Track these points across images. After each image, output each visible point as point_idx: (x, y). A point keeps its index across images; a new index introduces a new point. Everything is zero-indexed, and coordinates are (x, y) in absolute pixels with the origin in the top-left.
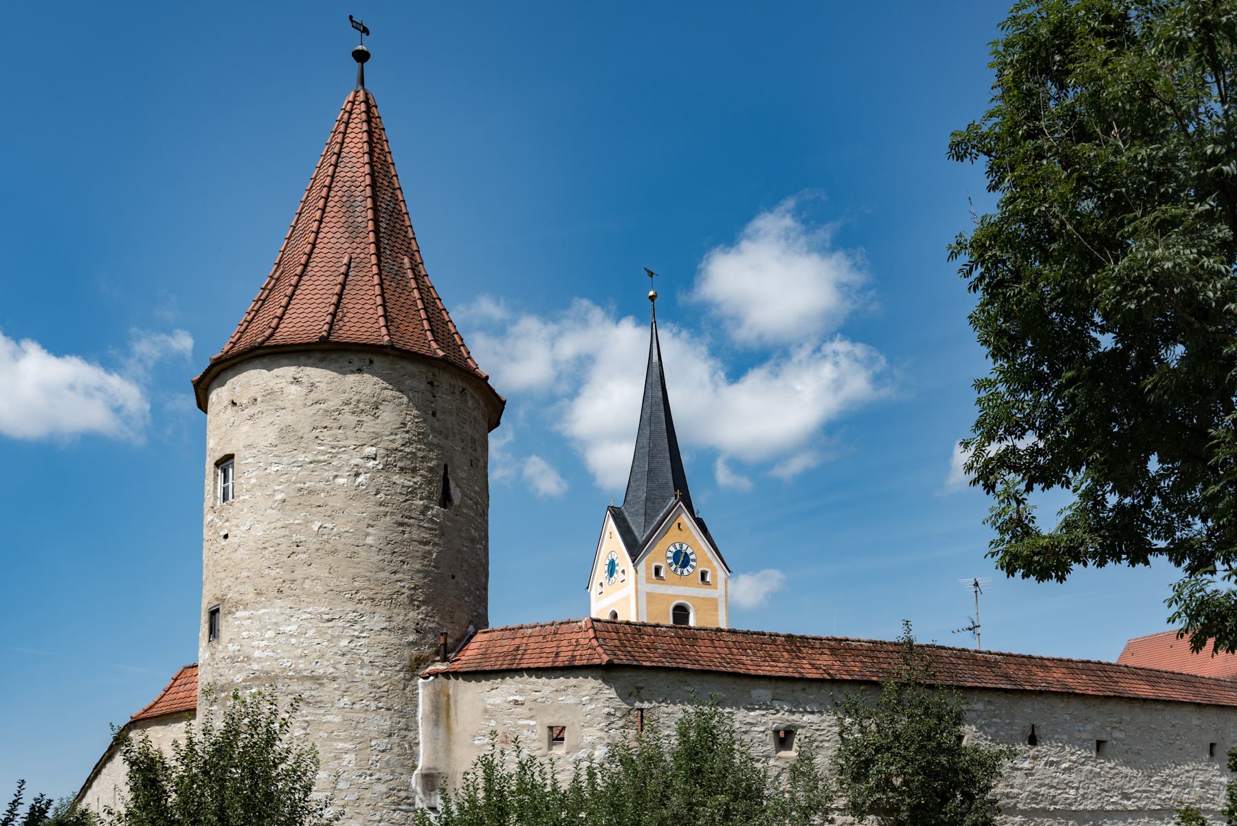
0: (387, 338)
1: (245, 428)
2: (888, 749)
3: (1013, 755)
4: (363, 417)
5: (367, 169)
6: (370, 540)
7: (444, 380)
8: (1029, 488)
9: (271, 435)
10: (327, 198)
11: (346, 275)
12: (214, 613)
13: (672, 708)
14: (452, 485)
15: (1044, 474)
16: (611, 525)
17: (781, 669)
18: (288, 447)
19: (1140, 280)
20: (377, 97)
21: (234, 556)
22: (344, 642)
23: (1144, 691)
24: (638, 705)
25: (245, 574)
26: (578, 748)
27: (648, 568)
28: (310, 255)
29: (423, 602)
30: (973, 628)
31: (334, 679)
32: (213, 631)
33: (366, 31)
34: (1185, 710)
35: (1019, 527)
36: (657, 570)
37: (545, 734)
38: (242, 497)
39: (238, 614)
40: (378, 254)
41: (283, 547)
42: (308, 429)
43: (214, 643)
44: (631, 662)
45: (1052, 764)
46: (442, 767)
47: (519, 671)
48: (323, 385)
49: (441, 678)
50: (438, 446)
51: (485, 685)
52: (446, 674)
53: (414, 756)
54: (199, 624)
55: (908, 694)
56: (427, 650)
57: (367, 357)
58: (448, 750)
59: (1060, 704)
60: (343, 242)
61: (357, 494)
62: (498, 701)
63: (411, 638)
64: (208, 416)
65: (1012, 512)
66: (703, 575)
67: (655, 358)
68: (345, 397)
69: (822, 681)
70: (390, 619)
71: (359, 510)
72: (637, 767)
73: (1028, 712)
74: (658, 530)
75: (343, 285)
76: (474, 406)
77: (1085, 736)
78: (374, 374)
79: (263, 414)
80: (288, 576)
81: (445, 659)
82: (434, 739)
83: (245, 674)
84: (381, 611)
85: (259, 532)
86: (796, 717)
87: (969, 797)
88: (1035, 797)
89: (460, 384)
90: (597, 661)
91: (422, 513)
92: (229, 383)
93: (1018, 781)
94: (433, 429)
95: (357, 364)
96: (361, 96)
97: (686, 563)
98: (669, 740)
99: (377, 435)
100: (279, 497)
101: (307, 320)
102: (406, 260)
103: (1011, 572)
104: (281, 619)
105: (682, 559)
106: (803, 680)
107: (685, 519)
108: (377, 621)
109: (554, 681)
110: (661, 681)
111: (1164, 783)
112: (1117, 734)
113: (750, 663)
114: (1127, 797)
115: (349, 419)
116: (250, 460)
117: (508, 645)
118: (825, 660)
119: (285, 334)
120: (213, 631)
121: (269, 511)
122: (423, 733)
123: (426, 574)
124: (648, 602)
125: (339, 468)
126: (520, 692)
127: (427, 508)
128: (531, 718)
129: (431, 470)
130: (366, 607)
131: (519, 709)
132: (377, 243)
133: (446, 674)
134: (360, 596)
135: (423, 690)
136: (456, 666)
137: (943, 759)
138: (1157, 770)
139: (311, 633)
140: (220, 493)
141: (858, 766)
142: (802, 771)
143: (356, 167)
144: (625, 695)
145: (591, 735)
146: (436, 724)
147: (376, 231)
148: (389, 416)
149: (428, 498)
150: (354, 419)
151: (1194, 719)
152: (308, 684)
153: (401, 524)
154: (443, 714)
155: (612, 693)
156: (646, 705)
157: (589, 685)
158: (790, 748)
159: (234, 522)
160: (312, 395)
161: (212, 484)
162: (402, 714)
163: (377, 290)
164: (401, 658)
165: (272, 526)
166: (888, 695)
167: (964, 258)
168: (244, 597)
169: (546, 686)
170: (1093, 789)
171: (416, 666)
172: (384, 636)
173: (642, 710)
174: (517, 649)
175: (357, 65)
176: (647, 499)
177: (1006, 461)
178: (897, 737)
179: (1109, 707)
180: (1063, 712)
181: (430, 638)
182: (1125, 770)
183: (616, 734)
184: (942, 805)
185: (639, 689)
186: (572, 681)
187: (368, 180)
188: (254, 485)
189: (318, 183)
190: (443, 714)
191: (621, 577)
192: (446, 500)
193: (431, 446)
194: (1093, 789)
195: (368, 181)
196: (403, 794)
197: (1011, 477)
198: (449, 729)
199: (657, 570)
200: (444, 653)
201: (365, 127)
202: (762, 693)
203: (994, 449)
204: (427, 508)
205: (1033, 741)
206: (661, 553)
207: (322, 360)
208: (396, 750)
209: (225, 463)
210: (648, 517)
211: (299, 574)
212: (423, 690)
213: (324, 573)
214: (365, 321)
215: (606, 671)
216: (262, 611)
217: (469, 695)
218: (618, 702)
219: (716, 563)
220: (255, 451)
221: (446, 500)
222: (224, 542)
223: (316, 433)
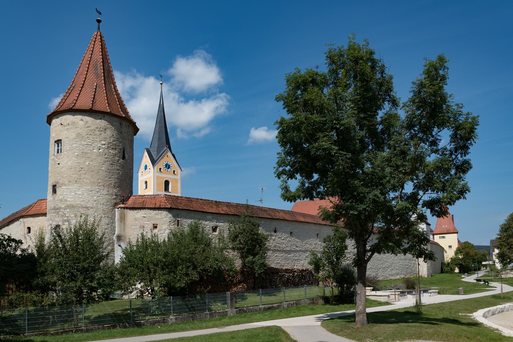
0: (109, 110)
1: (65, 132)
2: (242, 233)
3: (272, 235)
4: (102, 132)
5: (101, 57)
6: (103, 168)
7: (124, 123)
8: (288, 179)
9: (74, 135)
10: (89, 64)
11: (96, 89)
12: (54, 186)
13: (186, 220)
14: (126, 153)
15: (291, 176)
16: (146, 154)
17: (214, 211)
18: (79, 139)
19: (320, 149)
20: (104, 35)
21: (61, 170)
22: (95, 198)
23: (302, 219)
24: (178, 219)
25: (65, 175)
26: (161, 230)
27: (157, 168)
28: (84, 81)
29: (117, 187)
30: (261, 201)
31: (92, 208)
32: (54, 191)
33: (100, 13)
34: (312, 225)
35: (286, 189)
36: (160, 169)
37: (152, 227)
38: (64, 152)
39: (63, 187)
40: (105, 83)
41: (77, 169)
42: (85, 135)
43: (55, 195)
44: (177, 207)
45: (279, 238)
46: (122, 234)
47: (145, 208)
48: (90, 122)
49: (123, 209)
50: (122, 142)
51: (135, 211)
52: (124, 208)
53: (114, 231)
54: (47, 190)
55: (247, 219)
56: (118, 201)
57: (103, 115)
58: (124, 229)
59: (282, 222)
60: (95, 80)
61: (100, 155)
62: (139, 216)
63: (114, 197)
64: (51, 126)
65: (284, 185)
66: (174, 172)
67: (162, 103)
68: (96, 126)
69: (225, 214)
70: (108, 191)
71: (101, 159)
72: (176, 237)
73: (275, 224)
74: (161, 156)
75: (95, 92)
76: (131, 130)
77: (288, 231)
78: (105, 120)
79: (70, 129)
80: (79, 177)
81: (123, 204)
82: (120, 226)
84: (106, 189)
85: (70, 163)
86: (218, 224)
87: (260, 246)
88: (275, 246)
89: (128, 124)
90: (167, 207)
91: (118, 161)
92: (60, 118)
93: (271, 242)
94: (121, 137)
95: (100, 117)
96: (99, 34)
97: (169, 168)
98: (186, 229)
99: (106, 138)
100: (76, 154)
101: (85, 102)
102: (112, 86)
103: (285, 200)
104: (76, 190)
105: (168, 166)
106: (220, 214)
107: (169, 154)
108: (105, 192)
109: (155, 212)
110: (184, 213)
111: (306, 244)
112: (295, 231)
113: (207, 209)
114: (297, 247)
115: (97, 133)
117: (141, 200)
118: (225, 208)
119: (78, 106)
120: (54, 191)
122: (117, 224)
123: (118, 179)
124: (378, 290)
125: (94, 147)
126: (145, 214)
127: (119, 160)
129: (120, 149)
130: (102, 188)
131: (145, 219)
132: (104, 80)
133: (124, 208)
134: (100, 184)
135: (117, 212)
136: (127, 206)
137: (256, 237)
138: (304, 240)
139: (85, 194)
140: (56, 150)
141: (234, 238)
142: (221, 239)
143: (98, 56)
144: (174, 216)
145: (165, 227)
146: (121, 222)
147: (104, 76)
148: (109, 133)
149: (119, 157)
150: (99, 133)
151: (314, 227)
152: (85, 209)
153: (112, 164)
154: (123, 219)
155: (170, 215)
156: (180, 219)
157: (165, 213)
158: (216, 232)
159: (62, 160)
160: (87, 125)
161: (53, 148)
162: (111, 218)
163: (105, 95)
164: (111, 203)
166: (242, 219)
167: (277, 126)
169: (153, 213)
170: (289, 244)
171: (115, 205)
172: (107, 196)
173: (178, 221)
174: (144, 201)
175: (98, 24)
176: (158, 147)
177: (283, 172)
178: (244, 230)
179: (294, 223)
180: (283, 224)
181: (119, 197)
182: (297, 240)
183: (172, 227)
184: (254, 249)
185: (178, 215)
186: (160, 212)
187: (101, 60)
189: (86, 59)
190: (123, 219)
191: (149, 170)
192: (124, 158)
193: (120, 142)
194: (289, 244)
195: (101, 61)
196: (111, 241)
197: (284, 176)
198: (124, 223)
199: (160, 169)
200: (123, 201)
201: (100, 44)
202: (209, 217)
203: (281, 169)
204: (119, 160)
205: (275, 232)
206: (161, 164)
207: (90, 115)
208: (110, 229)
209: (58, 142)
210: (158, 152)
211: (82, 177)
212: (117, 212)
213: (90, 177)
214: (102, 105)
215: (169, 210)
217: (131, 214)
218: (172, 218)
219: (178, 168)
221: (124, 158)
222: (58, 166)
223: (88, 136)
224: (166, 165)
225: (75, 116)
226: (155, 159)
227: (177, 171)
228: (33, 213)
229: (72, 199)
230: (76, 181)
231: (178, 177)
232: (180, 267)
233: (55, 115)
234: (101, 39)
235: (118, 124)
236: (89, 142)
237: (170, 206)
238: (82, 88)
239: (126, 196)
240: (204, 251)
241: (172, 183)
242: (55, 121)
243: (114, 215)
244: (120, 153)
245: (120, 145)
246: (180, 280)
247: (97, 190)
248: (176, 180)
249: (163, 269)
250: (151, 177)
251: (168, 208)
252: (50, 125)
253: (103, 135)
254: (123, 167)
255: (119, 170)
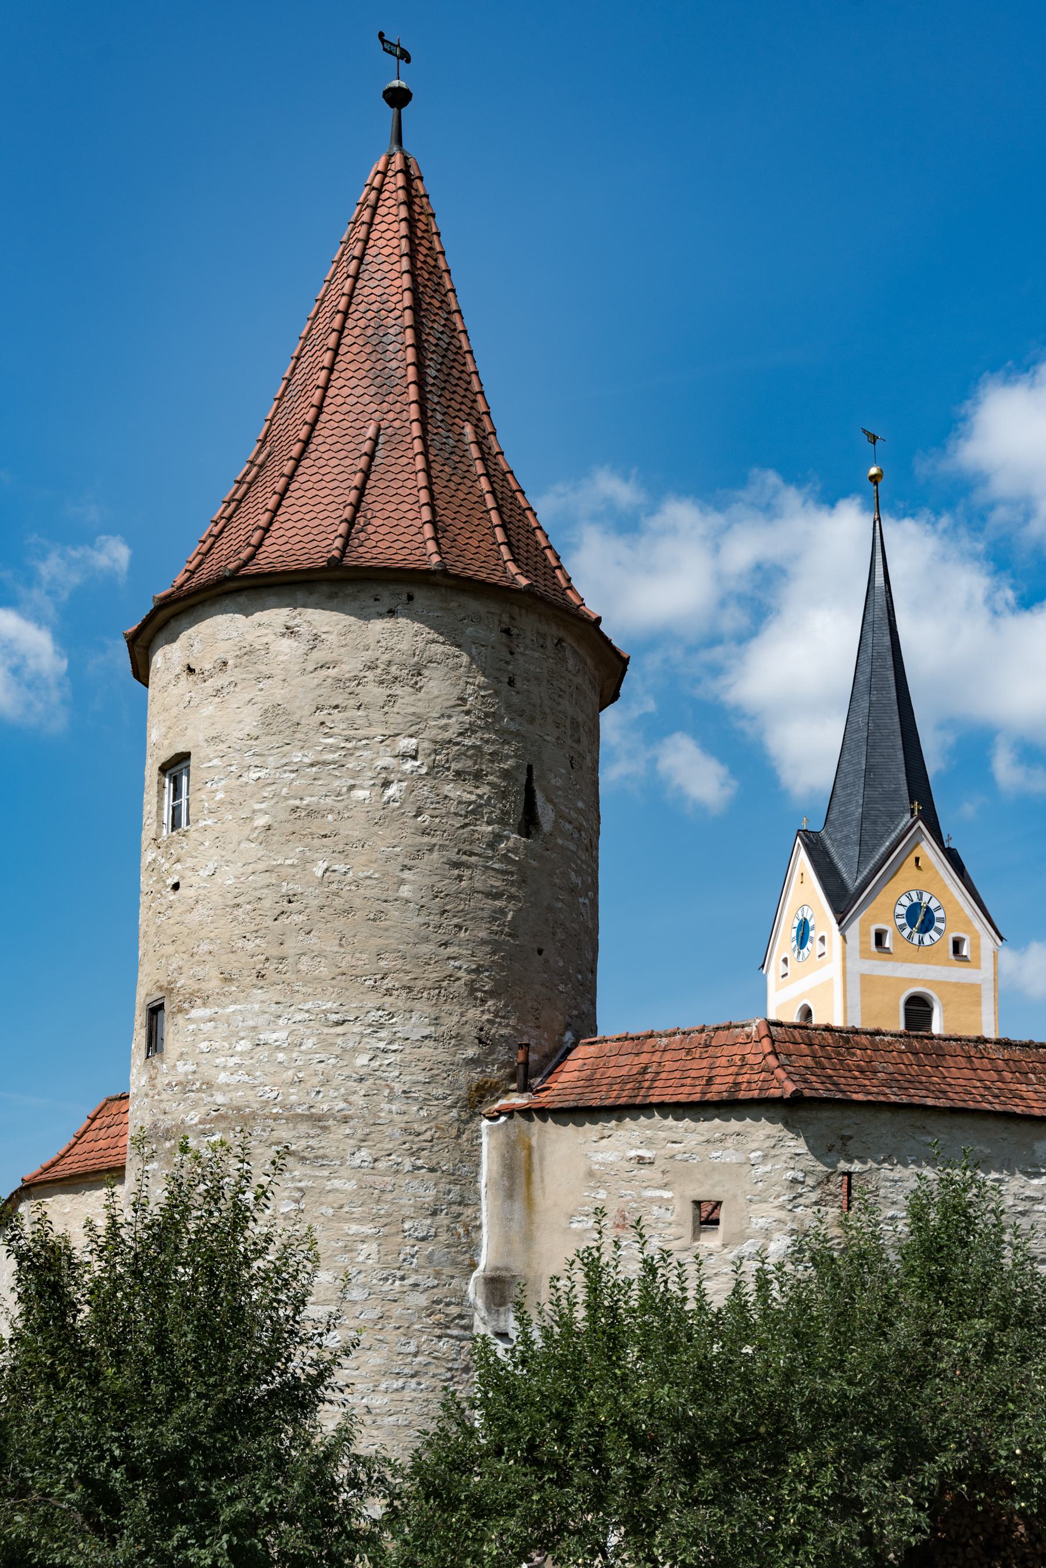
0: (435, 558)
4: (397, 690)
5: (406, 281)
6: (405, 891)
7: (529, 625)
9: (250, 721)
10: (341, 331)
12: (155, 1011)
13: (899, 1172)
14: (540, 799)
16: (802, 861)
18: (276, 740)
20: (422, 164)
21: (188, 918)
22: (363, 1060)
24: (843, 1166)
25: (205, 947)
27: (863, 933)
28: (313, 425)
29: (491, 994)
31: (346, 1120)
32: (154, 1042)
33: (405, 56)
36: (880, 937)
39: (194, 1013)
40: (423, 421)
41: (267, 903)
42: (308, 710)
43: (155, 1060)
44: (833, 1094)
46: (517, 1266)
47: (646, 1109)
49: (519, 1120)
50: (517, 735)
51: (591, 1130)
52: (527, 1113)
53: (473, 1247)
56: (495, 1073)
57: (405, 590)
58: (528, 1238)
60: (369, 402)
61: (384, 815)
62: (611, 1157)
63: (471, 1052)
64: (150, 690)
66: (957, 944)
67: (879, 580)
68: (367, 656)
70: (436, 1021)
71: (388, 841)
74: (881, 868)
75: (367, 473)
78: (414, 617)
79: (237, 689)
80: (274, 951)
81: (525, 1088)
82: (506, 1220)
83: (203, 1110)
85: (228, 878)
89: (554, 631)
90: (776, 1093)
91: (492, 846)
92: (183, 637)
94: (509, 706)
95: (387, 602)
96: (397, 163)
98: (894, 1226)
99: (419, 718)
100: (261, 821)
101: (306, 532)
102: (468, 429)
104: (262, 1020)
105: (921, 919)
107: (928, 850)
108: (415, 1025)
109: (704, 1126)
110: (881, 1126)
115: (373, 692)
116: (216, 762)
117: (628, 1065)
119: (276, 554)
120: (154, 1042)
121: (245, 845)
122: (487, 1209)
123: (496, 946)
125: (357, 774)
126: (648, 1143)
127: (498, 838)
128: (665, 1186)
129: (505, 774)
130: (399, 1001)
131: (645, 1172)
133: (527, 1113)
134: (388, 983)
136: (544, 1099)
139: (308, 1044)
140: (167, 816)
143: (389, 278)
144: (823, 1150)
145: (765, 1215)
146: (510, 1194)
147: (420, 383)
148: (439, 686)
149: (502, 821)
150: (382, 692)
152: (303, 1128)
153: (456, 865)
154: (521, 1179)
155: (799, 1146)
156: (856, 1167)
157: (762, 1132)
160: (316, 655)
162: (454, 1177)
164: (453, 1086)
165: (250, 869)
168: (204, 986)
171: (477, 1099)
172: (427, 1049)
173: (849, 1174)
174: (644, 1071)
175: (392, 112)
176: (864, 817)
181: (502, 1053)
186: (734, 1125)
187: (407, 299)
188: (222, 802)
189: (328, 308)
190: (521, 1179)
192: (529, 823)
193: (506, 736)
196: (454, 1310)
198: (530, 1203)
199: (880, 937)
200: (524, 1077)
201: (403, 213)
204: (498, 838)
206: (885, 908)
207: (331, 597)
208: (444, 1237)
209: (176, 766)
210: (865, 847)
211: (291, 947)
212: (489, 1138)
214: (401, 534)
215: (790, 1110)
216: (231, 1008)
217: (564, 1148)
218: (810, 1161)
219: (979, 924)
220: (223, 746)
221: (529, 823)
222: (172, 896)
223: (321, 716)
224: (913, 911)
225: (258, 616)
226: (852, 885)
227: (976, 937)
228: (76, 1168)
229: (241, 1076)
230: (260, 976)
231: (982, 975)
232: (802, 1460)
233: (161, 628)
234: (408, 187)
235: (494, 636)
236: (326, 748)
237: (790, 1088)
238: (298, 460)
239: (547, 1048)
240: (989, 1354)
241: (945, 1007)
242: (166, 659)
243: (472, 1156)
244: (503, 795)
245: (506, 750)
246: (453, 1505)
247: (374, 1015)
248: (973, 991)
249: (690, 1469)
250: (829, 984)
251: (779, 1101)
252: (147, 686)
253: (407, 701)
254: (522, 875)
255: (497, 896)
